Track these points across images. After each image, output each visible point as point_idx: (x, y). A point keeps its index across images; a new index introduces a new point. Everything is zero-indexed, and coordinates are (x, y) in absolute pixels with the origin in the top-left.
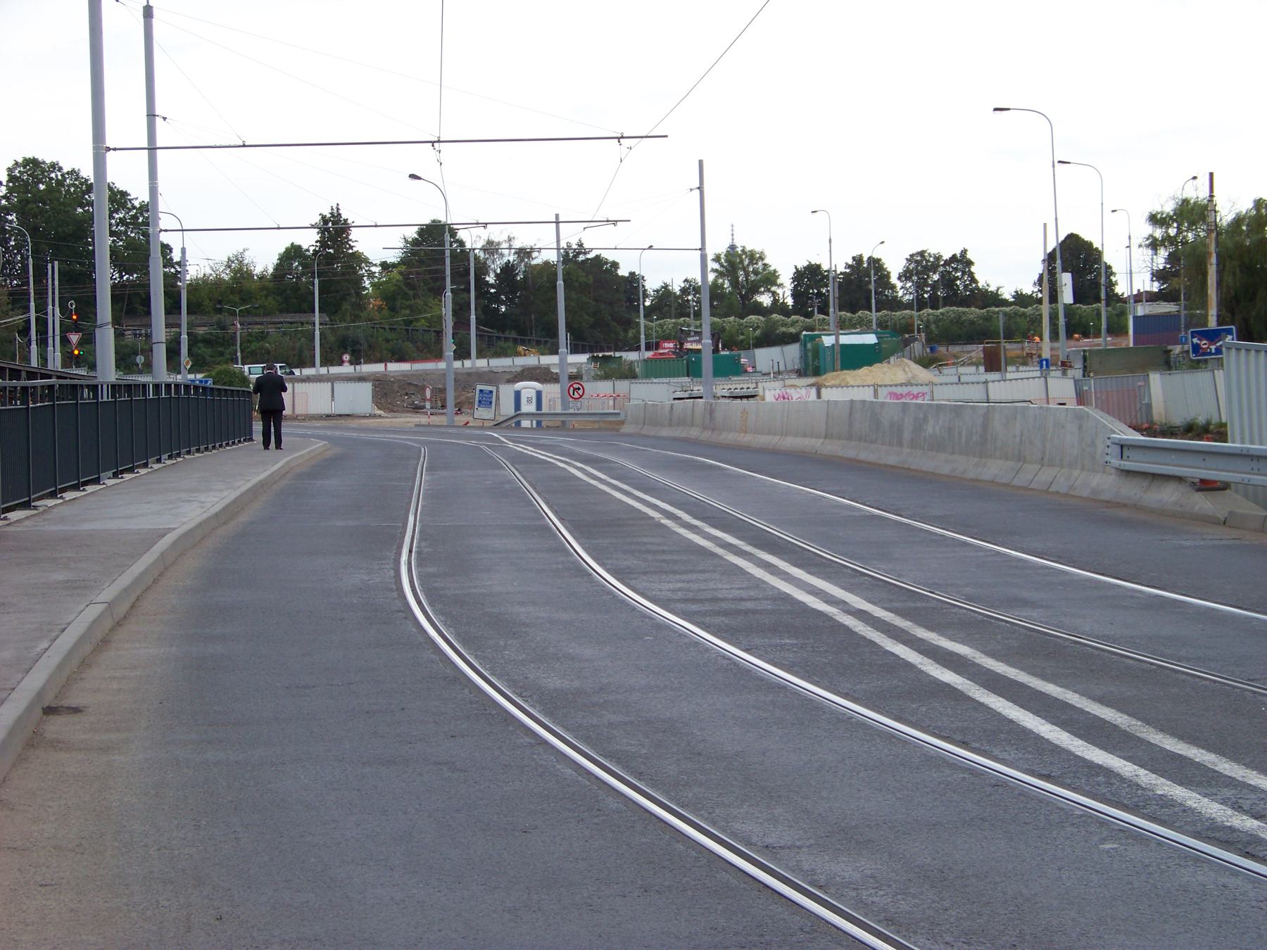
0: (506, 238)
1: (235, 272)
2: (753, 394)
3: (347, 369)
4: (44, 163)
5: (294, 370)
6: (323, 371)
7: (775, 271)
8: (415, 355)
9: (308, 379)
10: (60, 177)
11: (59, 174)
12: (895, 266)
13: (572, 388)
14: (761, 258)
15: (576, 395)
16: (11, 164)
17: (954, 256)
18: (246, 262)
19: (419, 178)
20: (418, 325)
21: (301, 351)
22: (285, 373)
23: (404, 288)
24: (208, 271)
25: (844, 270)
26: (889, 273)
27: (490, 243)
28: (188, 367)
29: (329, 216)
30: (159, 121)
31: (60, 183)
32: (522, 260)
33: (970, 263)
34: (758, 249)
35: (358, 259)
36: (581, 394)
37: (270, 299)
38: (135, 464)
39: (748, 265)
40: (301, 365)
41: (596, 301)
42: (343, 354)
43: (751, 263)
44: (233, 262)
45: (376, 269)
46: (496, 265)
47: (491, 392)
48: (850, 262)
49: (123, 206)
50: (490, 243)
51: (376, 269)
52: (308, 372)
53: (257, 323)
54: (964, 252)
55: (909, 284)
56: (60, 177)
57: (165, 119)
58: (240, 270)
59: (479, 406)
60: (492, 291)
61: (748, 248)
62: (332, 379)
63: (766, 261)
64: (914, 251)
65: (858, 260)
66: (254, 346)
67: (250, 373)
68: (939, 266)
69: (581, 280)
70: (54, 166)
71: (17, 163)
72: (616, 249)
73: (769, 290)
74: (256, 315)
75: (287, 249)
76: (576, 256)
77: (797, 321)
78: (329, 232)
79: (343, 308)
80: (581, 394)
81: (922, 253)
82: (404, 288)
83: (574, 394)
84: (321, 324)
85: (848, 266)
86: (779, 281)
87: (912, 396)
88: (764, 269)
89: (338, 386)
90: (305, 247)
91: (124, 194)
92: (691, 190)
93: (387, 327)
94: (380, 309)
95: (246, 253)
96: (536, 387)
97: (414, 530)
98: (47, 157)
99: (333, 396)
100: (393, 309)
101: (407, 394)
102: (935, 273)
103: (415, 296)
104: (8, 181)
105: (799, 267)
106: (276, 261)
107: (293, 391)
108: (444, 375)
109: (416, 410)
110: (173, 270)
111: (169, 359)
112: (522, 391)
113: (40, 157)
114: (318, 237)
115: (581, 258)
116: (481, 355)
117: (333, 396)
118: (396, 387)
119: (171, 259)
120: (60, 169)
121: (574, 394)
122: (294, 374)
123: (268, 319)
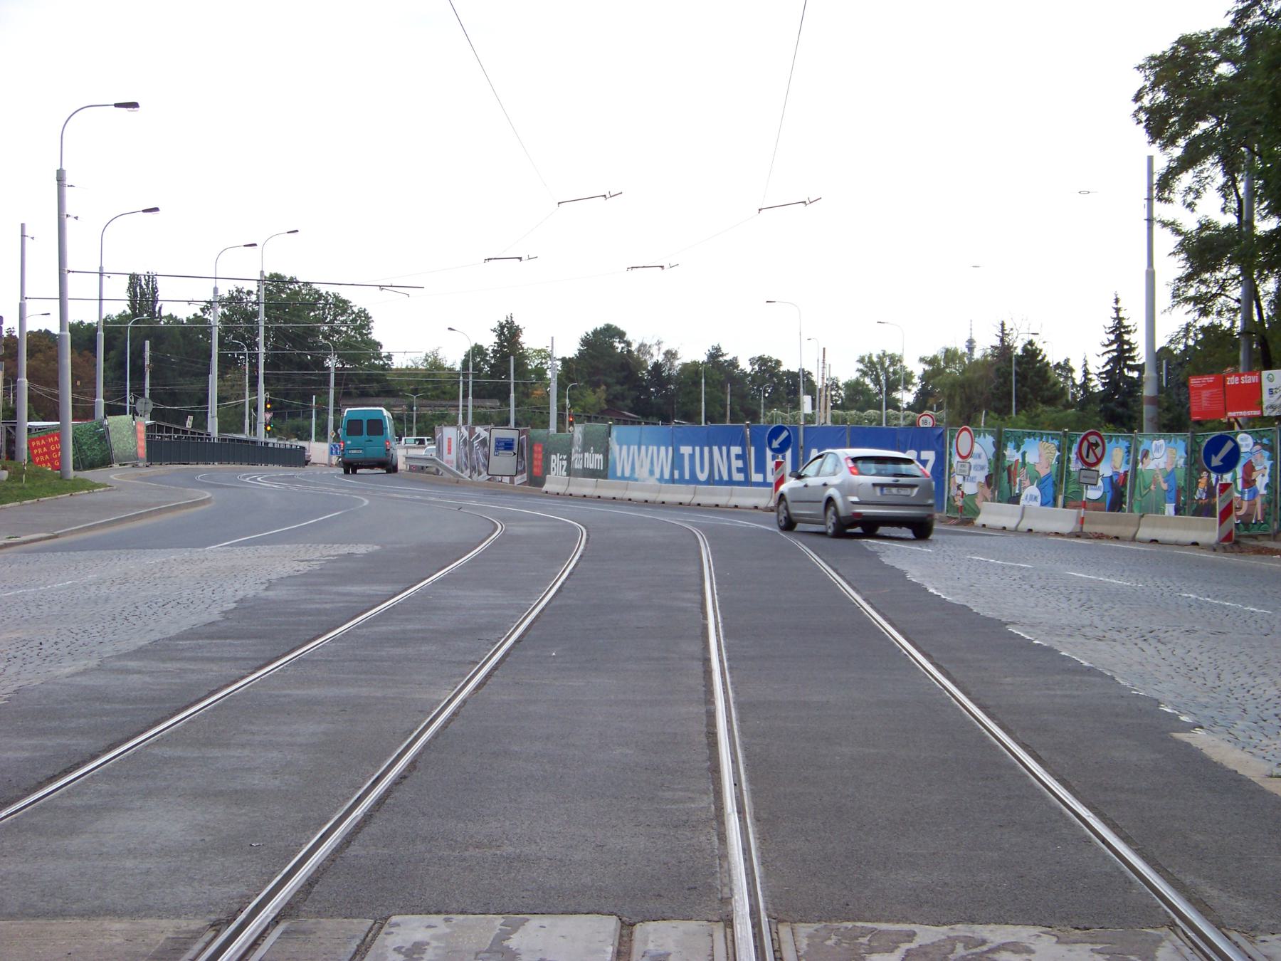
0: (656, 341)
1: (431, 364)
10: (297, 289)
17: (1058, 364)
18: (439, 357)
29: (505, 322)
30: (27, 240)
31: (297, 293)
34: (898, 353)
36: (1099, 456)
39: (889, 366)
44: (430, 357)
49: (344, 312)
54: (1067, 361)
56: (297, 289)
57: (33, 238)
74: (444, 399)
77: (908, 416)
78: (504, 335)
80: (1099, 456)
83: (1087, 456)
84: (458, 406)
90: (485, 347)
91: (345, 302)
95: (440, 350)
97: (709, 561)
98: (287, 273)
108: (307, 463)
113: (282, 272)
119: (380, 354)
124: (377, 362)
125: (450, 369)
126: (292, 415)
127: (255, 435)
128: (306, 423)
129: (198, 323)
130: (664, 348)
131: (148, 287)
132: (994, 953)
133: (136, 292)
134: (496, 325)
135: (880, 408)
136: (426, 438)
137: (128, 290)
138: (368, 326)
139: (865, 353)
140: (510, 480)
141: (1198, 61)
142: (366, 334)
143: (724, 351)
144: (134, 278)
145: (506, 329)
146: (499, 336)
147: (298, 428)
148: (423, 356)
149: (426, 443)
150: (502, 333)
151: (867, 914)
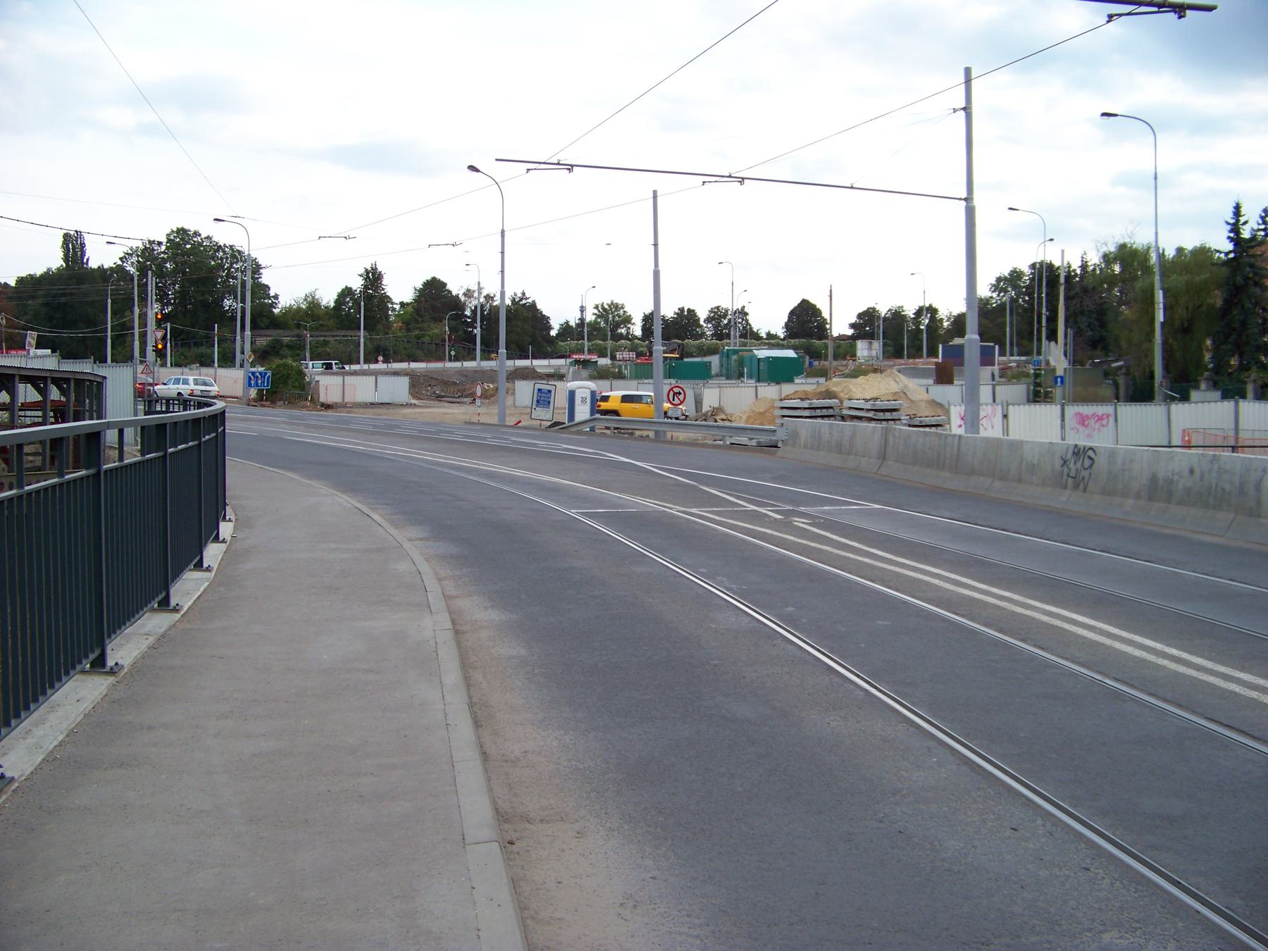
1: (310, 303)
2: (895, 408)
3: (381, 366)
4: (189, 231)
5: (345, 366)
6: (366, 367)
7: (630, 315)
8: (423, 358)
9: (355, 373)
10: (200, 240)
11: (199, 238)
12: (702, 314)
13: (672, 392)
14: (622, 308)
15: (677, 401)
16: (168, 231)
19: (477, 170)
20: (426, 339)
21: (350, 353)
22: (339, 368)
23: (415, 316)
24: (293, 303)
25: (673, 316)
26: (699, 318)
27: (468, 290)
28: (250, 360)
29: (370, 269)
31: (200, 244)
32: (488, 302)
33: (746, 314)
35: (386, 299)
37: (331, 321)
38: (203, 440)
40: (350, 362)
41: (533, 328)
42: (377, 356)
43: (616, 310)
44: (308, 297)
45: (397, 307)
46: (473, 303)
47: (550, 391)
48: (677, 311)
50: (468, 290)
51: (397, 307)
52: (355, 367)
53: (322, 336)
55: (710, 325)
56: (200, 240)
58: (313, 302)
59: (537, 406)
60: (469, 320)
61: (615, 302)
62: (376, 374)
63: (625, 309)
64: (713, 306)
65: (682, 310)
66: (320, 350)
67: (313, 368)
68: (727, 315)
69: (524, 314)
70: (196, 234)
71: (173, 231)
72: (852, 188)
73: (626, 326)
74: (322, 331)
75: (343, 290)
76: (521, 300)
78: (370, 279)
79: (378, 328)
81: (718, 308)
82: (415, 316)
83: (673, 400)
85: (675, 313)
86: (632, 322)
87: (1096, 418)
88: (624, 314)
89: (380, 379)
90: (354, 288)
92: (955, 110)
93: (405, 340)
94: (401, 328)
96: (591, 387)
99: (376, 387)
100: (408, 330)
101: (430, 386)
102: (725, 319)
103: (423, 322)
104: (167, 243)
105: (646, 313)
106: (336, 297)
107: (344, 382)
109: (440, 399)
110: (270, 301)
111: (637, 402)
112: (577, 391)
114: (362, 282)
115: (524, 302)
116: (365, 362)
117: (376, 387)
118: (422, 381)
120: (200, 235)
121: (673, 400)
122: (344, 368)
123: (330, 334)
124: (266, 301)
125: (326, 307)
126: (198, 345)
127: (1008, 436)
128: (209, 351)
129: (119, 270)
130: (485, 293)
131: (77, 243)
132: (85, 255)
133: (69, 248)
134: (362, 271)
135: (605, 340)
136: (333, 362)
137: (62, 246)
138: (259, 271)
139: (599, 302)
140: (505, 421)
141: (348, 314)
142: (258, 278)
143: (527, 296)
144: (67, 237)
145: (371, 274)
146: (366, 279)
147: (202, 355)
148: (303, 296)
149: (334, 367)
150: (368, 277)
151: (178, 322)
